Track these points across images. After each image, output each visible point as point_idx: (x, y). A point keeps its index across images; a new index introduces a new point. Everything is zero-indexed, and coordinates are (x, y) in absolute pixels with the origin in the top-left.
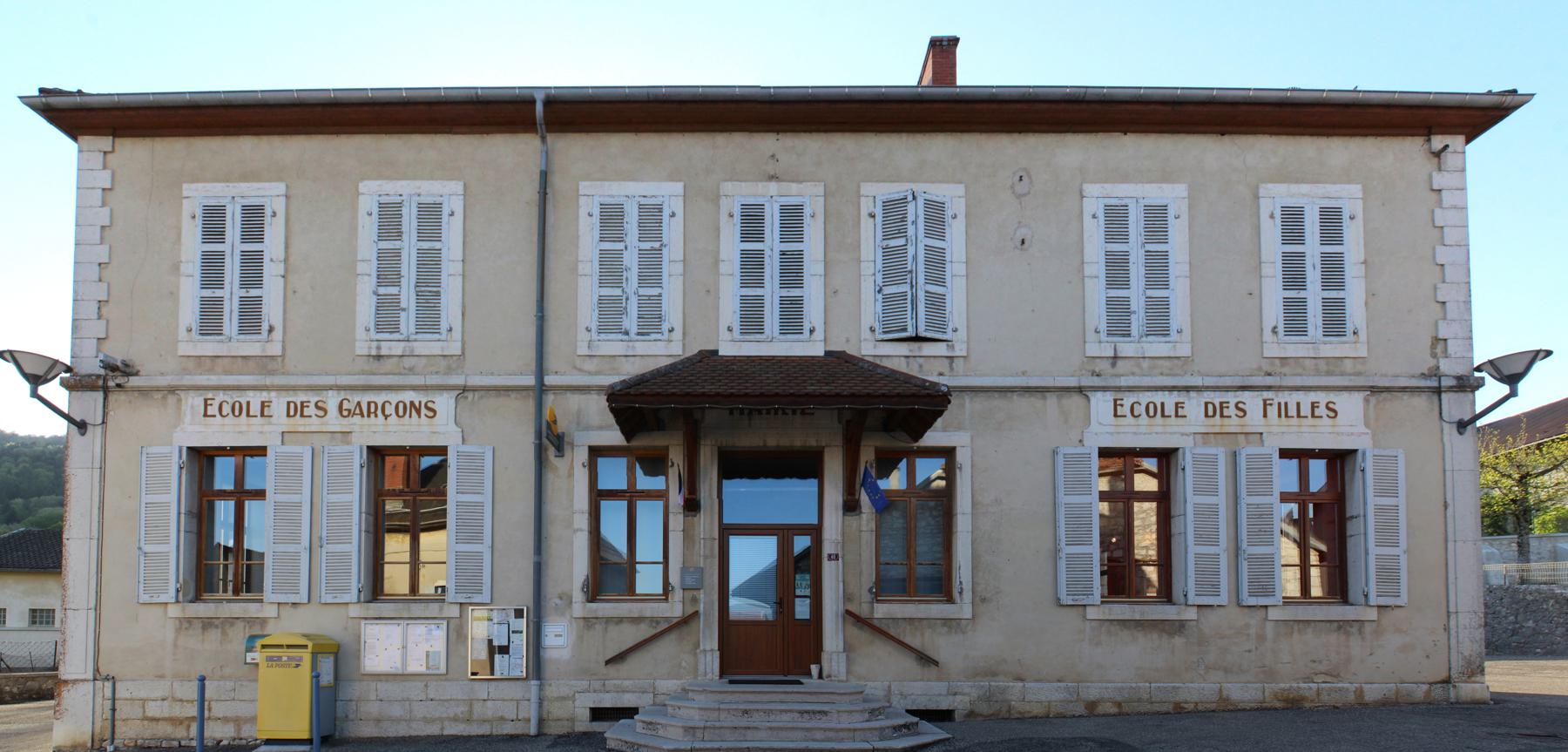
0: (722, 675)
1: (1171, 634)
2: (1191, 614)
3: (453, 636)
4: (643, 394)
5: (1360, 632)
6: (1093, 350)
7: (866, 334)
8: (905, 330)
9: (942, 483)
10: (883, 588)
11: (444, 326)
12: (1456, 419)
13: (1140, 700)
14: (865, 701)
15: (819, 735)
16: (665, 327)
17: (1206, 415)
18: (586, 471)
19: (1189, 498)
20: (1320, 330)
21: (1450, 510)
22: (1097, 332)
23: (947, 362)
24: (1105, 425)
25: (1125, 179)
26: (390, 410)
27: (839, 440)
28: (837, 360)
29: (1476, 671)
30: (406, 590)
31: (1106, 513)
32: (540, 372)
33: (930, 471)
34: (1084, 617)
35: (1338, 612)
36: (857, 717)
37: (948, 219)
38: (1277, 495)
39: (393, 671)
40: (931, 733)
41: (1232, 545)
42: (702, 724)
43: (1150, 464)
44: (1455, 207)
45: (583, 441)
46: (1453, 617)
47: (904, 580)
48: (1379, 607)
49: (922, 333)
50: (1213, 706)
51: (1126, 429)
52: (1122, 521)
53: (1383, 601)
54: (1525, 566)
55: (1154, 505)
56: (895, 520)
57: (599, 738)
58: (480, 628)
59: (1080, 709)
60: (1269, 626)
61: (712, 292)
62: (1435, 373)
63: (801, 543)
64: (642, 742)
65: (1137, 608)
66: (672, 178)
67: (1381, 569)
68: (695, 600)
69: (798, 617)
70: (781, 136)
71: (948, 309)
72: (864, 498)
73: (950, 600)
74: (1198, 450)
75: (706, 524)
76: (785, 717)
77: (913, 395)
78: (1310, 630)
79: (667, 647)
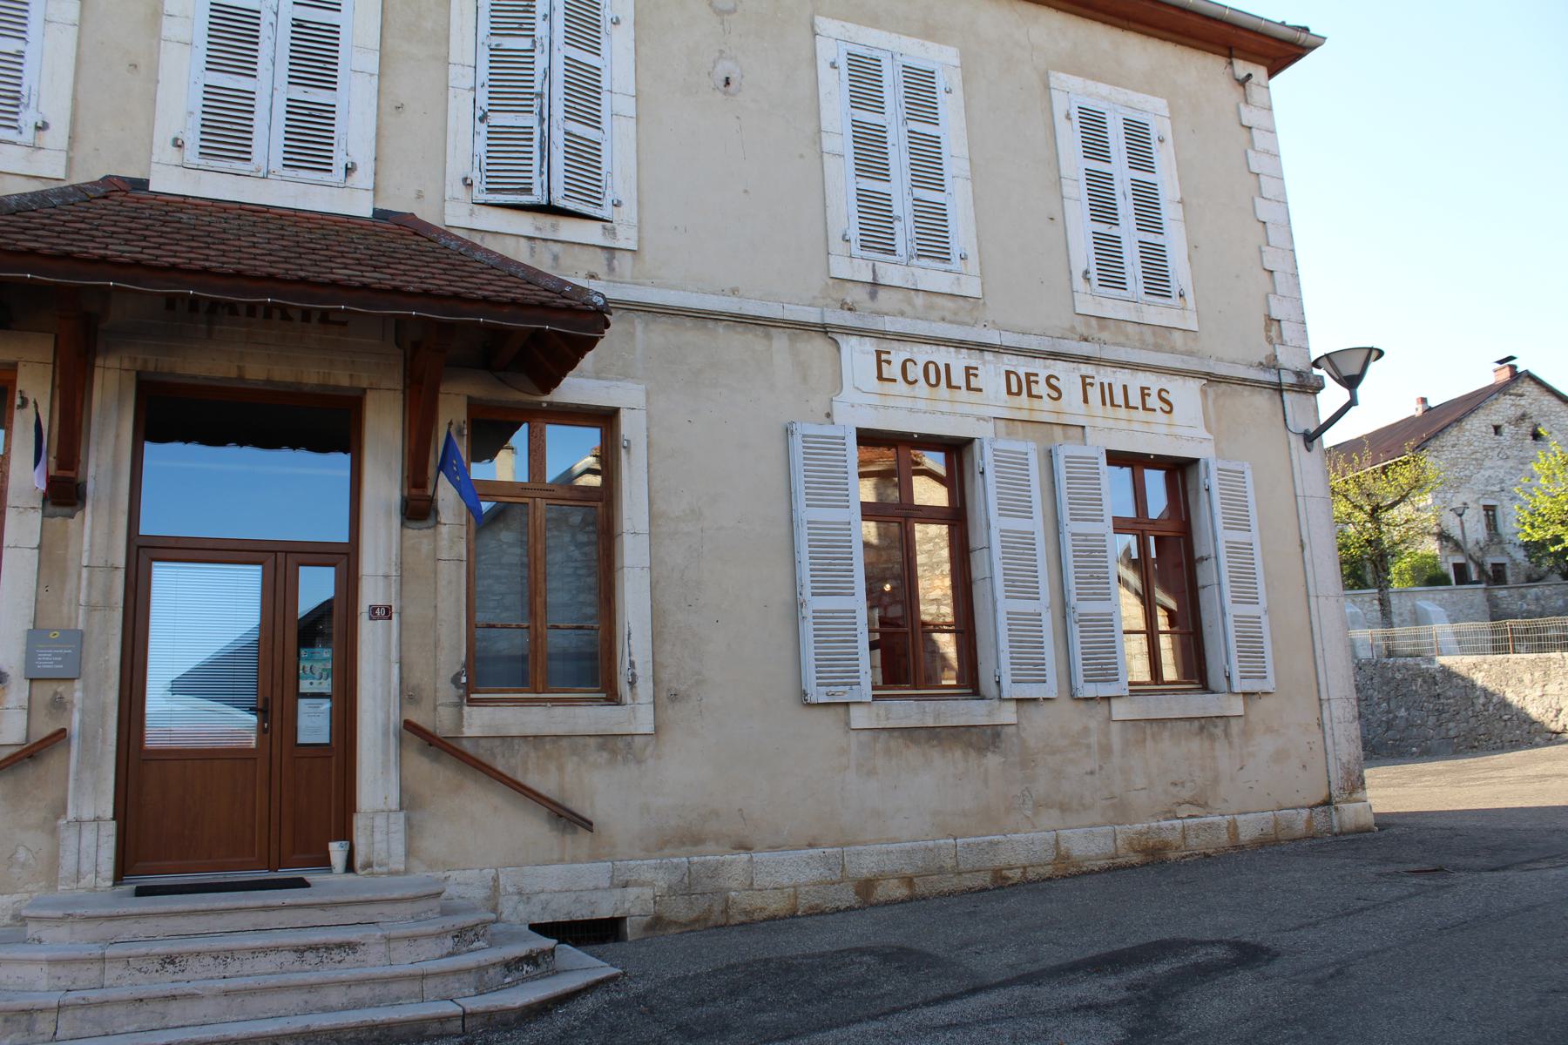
0: (120, 876)
1: (981, 751)
2: (1008, 714)
5: (1227, 734)
6: (841, 268)
7: (455, 189)
8: (528, 191)
9: (596, 481)
10: (482, 676)
13: (941, 870)
14: (445, 912)
15: (335, 997)
16: (28, 118)
17: (1009, 392)
19: (995, 523)
20: (1141, 285)
21: (1307, 552)
23: (602, 256)
24: (866, 396)
25: (874, 21)
27: (396, 380)
28: (397, 230)
29: (1356, 785)
31: (874, 539)
33: (571, 453)
34: (848, 724)
35: (1197, 704)
36: (429, 948)
37: (605, 24)
40: (582, 967)
41: (1057, 600)
43: (934, 461)
46: (1325, 705)
47: (524, 659)
48: (1244, 694)
49: (559, 202)
50: (1047, 871)
52: (897, 555)
53: (1248, 686)
54: (1388, 632)
55: (944, 529)
59: (848, 897)
60: (1115, 727)
61: (144, 68)
62: (1272, 364)
63: (315, 587)
65: (929, 706)
67: (1242, 637)
68: (59, 705)
69: (303, 738)
72: (446, 494)
73: (613, 698)
74: (1002, 444)
75: (97, 535)
76: (264, 964)
78: (1166, 734)
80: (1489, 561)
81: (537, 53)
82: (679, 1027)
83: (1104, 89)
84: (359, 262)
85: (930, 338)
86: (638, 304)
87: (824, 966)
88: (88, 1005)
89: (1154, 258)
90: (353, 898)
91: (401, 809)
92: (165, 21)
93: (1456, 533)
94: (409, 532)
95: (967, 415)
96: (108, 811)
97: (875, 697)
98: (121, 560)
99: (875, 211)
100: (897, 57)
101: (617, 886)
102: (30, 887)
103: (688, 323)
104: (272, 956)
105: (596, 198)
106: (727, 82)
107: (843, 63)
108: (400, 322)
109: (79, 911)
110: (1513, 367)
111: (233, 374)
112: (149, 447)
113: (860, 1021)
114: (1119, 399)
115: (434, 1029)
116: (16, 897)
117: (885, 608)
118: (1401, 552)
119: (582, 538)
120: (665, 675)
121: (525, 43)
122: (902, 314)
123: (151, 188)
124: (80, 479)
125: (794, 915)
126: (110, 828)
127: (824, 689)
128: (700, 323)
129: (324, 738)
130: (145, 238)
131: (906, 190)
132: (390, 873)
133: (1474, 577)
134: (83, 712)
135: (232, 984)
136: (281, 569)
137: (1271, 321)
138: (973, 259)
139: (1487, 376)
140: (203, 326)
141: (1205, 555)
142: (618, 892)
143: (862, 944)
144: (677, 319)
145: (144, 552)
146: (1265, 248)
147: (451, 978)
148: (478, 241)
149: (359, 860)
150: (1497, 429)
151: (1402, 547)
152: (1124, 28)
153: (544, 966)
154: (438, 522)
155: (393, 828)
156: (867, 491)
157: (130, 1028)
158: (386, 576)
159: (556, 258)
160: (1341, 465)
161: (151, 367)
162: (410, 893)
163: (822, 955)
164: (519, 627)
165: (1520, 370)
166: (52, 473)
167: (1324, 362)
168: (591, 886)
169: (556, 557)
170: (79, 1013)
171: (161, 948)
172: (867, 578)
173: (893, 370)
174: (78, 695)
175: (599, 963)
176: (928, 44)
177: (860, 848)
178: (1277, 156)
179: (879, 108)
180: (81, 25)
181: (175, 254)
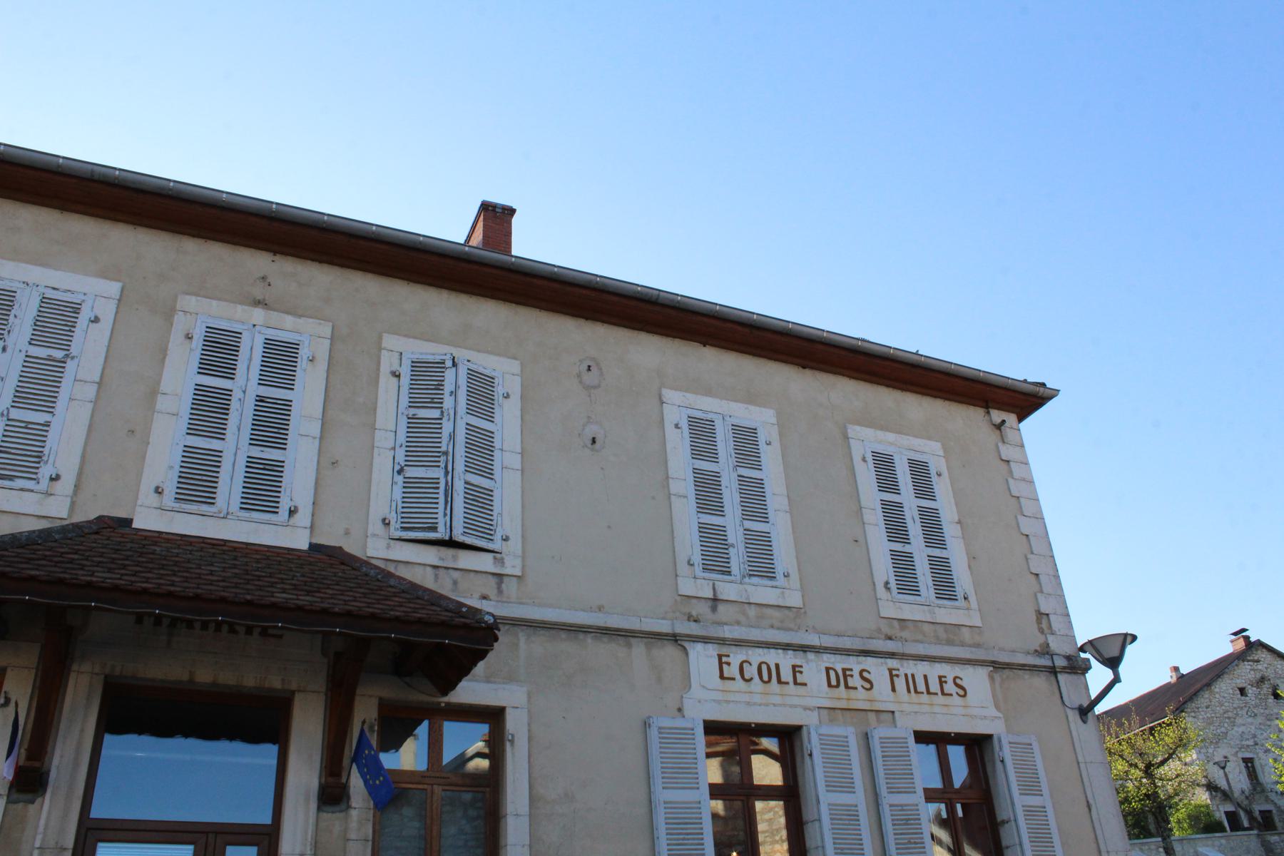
6: (687, 587)
7: (376, 527)
8: (434, 529)
9: (484, 764)
12: (1077, 705)
16: (45, 471)
19: (824, 799)
20: (932, 591)
22: (690, 564)
23: (492, 581)
24: (711, 693)
25: (708, 392)
27: (320, 683)
28: (327, 560)
33: (464, 742)
38: (921, 793)
43: (770, 743)
44: (1024, 480)
49: (460, 538)
51: (738, 697)
52: (740, 823)
56: (406, 822)
61: (139, 434)
62: (1045, 651)
66: (104, 274)
70: (278, 257)
72: (356, 783)
74: (824, 730)
77: (443, 624)
80: (1257, 808)
81: (444, 421)
83: (891, 437)
84: (295, 587)
85: (762, 643)
89: (941, 569)
92: (160, 397)
93: (1223, 784)
94: (324, 815)
95: (796, 706)
98: (70, 842)
99: (713, 540)
100: (727, 418)
103: (563, 635)
105: (488, 534)
106: (594, 441)
107: (684, 424)
110: (1247, 638)
111: (185, 677)
112: (108, 738)
114: (921, 687)
118: (1177, 804)
119: (472, 813)
121: (436, 414)
122: (738, 623)
123: (135, 525)
130: (124, 567)
131: (738, 523)
133: (1246, 824)
137: (1041, 615)
138: (795, 576)
139: (1225, 647)
141: (1005, 818)
146: (1030, 556)
150: (1242, 691)
151: (1176, 799)
152: (903, 390)
159: (455, 583)
160: (1114, 729)
165: (1252, 639)
166: (21, 763)
167: (1089, 647)
172: (716, 845)
173: (732, 670)
176: (752, 408)
178: (1032, 482)
179: (714, 457)
180: (96, 402)
181: (147, 580)
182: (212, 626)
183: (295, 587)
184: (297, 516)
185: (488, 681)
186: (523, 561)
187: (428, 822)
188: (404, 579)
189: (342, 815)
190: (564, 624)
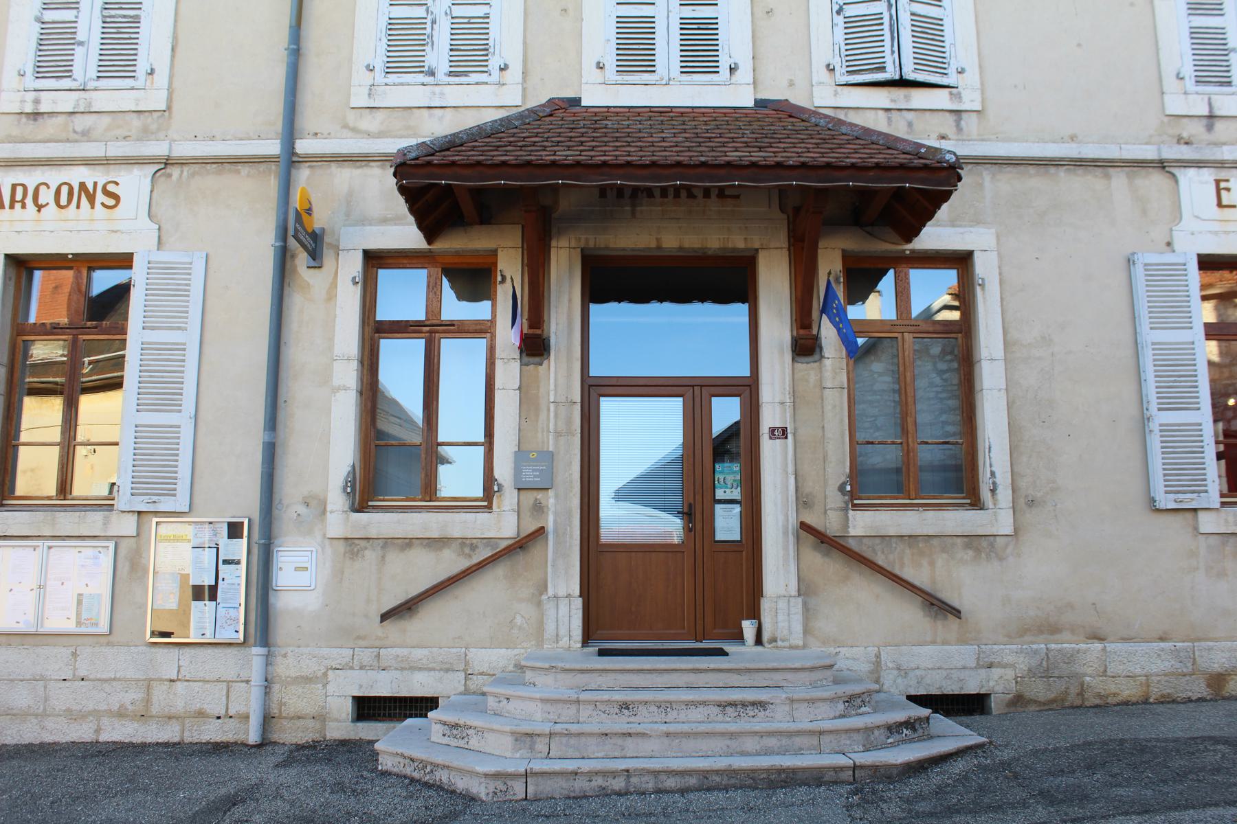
0: (587, 639)
3: (124, 568)
4: (453, 163)
6: (1175, 105)
7: (821, 74)
8: (882, 69)
9: (955, 315)
10: (862, 486)
11: (142, 67)
14: (836, 681)
15: (750, 744)
16: (494, 63)
18: (358, 290)
23: (951, 119)
26: (46, 196)
28: (776, 114)
30: (51, 488)
31: (1215, 358)
32: (290, 134)
33: (932, 292)
34: (1196, 528)
36: (824, 710)
39: (22, 628)
40: (952, 735)
42: (546, 728)
45: (353, 244)
47: (898, 471)
49: (910, 75)
57: (356, 753)
58: (178, 554)
59: (1199, 689)
63: (725, 413)
64: (439, 760)
68: (538, 508)
69: (720, 536)
71: (948, 40)
72: (828, 333)
73: (976, 503)
75: (559, 377)
76: (696, 714)
77: (902, 167)
79: (489, 591)
82: (1041, 793)
84: (747, 145)
86: (985, 158)
87: (1178, 751)
88: (569, 735)
90: (762, 666)
91: (799, 595)
94: (799, 366)
96: (576, 590)
97: (1223, 504)
101: (982, 667)
102: (525, 645)
103: (1032, 170)
104: (701, 709)
108: (782, 191)
109: (560, 665)
111: (653, 245)
112: (594, 308)
113: (1216, 805)
115: (830, 776)
116: (516, 651)
117: (1229, 421)
119: (942, 366)
120: (1022, 483)
123: (583, 104)
124: (545, 336)
125: (1146, 702)
126: (579, 602)
127: (1172, 496)
128: (1042, 169)
129: (736, 536)
132: (791, 647)
134: (556, 514)
135: (672, 728)
136: (698, 400)
140: (628, 208)
142: (983, 672)
143: (1216, 733)
144: (1022, 168)
145: (595, 390)
147: (844, 736)
148: (842, 117)
149: (766, 636)
153: (920, 731)
154: (822, 357)
155: (793, 610)
156: (1208, 313)
157: (600, 755)
158: (782, 403)
159: (910, 125)
161: (591, 245)
162: (808, 664)
163: (1176, 740)
164: (893, 443)
166: (525, 331)
168: (959, 665)
169: (921, 383)
170: (564, 740)
171: (619, 697)
172: (1212, 394)
174: (552, 501)
175: (968, 732)
177: (1211, 644)
182: (671, 192)
183: (747, 145)
184: (738, 73)
185: (953, 226)
186: (983, 93)
187: (901, 369)
188: (856, 126)
189: (816, 364)
190: (1033, 159)
